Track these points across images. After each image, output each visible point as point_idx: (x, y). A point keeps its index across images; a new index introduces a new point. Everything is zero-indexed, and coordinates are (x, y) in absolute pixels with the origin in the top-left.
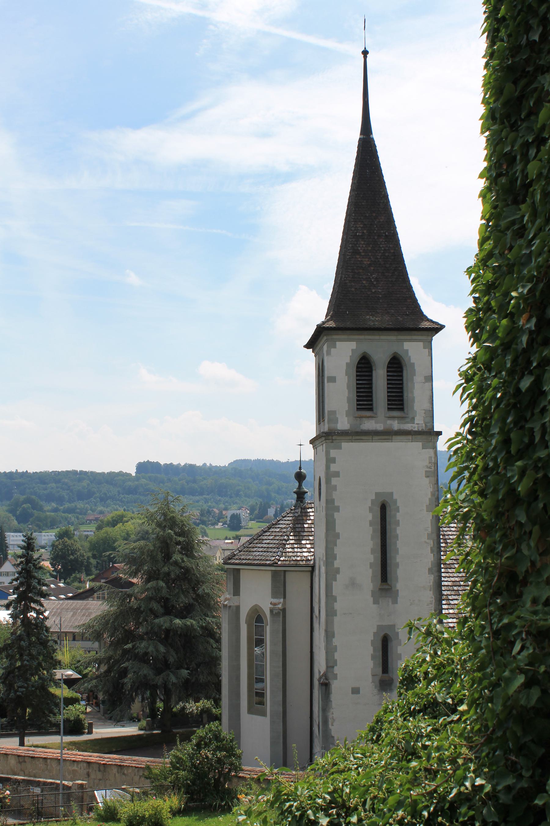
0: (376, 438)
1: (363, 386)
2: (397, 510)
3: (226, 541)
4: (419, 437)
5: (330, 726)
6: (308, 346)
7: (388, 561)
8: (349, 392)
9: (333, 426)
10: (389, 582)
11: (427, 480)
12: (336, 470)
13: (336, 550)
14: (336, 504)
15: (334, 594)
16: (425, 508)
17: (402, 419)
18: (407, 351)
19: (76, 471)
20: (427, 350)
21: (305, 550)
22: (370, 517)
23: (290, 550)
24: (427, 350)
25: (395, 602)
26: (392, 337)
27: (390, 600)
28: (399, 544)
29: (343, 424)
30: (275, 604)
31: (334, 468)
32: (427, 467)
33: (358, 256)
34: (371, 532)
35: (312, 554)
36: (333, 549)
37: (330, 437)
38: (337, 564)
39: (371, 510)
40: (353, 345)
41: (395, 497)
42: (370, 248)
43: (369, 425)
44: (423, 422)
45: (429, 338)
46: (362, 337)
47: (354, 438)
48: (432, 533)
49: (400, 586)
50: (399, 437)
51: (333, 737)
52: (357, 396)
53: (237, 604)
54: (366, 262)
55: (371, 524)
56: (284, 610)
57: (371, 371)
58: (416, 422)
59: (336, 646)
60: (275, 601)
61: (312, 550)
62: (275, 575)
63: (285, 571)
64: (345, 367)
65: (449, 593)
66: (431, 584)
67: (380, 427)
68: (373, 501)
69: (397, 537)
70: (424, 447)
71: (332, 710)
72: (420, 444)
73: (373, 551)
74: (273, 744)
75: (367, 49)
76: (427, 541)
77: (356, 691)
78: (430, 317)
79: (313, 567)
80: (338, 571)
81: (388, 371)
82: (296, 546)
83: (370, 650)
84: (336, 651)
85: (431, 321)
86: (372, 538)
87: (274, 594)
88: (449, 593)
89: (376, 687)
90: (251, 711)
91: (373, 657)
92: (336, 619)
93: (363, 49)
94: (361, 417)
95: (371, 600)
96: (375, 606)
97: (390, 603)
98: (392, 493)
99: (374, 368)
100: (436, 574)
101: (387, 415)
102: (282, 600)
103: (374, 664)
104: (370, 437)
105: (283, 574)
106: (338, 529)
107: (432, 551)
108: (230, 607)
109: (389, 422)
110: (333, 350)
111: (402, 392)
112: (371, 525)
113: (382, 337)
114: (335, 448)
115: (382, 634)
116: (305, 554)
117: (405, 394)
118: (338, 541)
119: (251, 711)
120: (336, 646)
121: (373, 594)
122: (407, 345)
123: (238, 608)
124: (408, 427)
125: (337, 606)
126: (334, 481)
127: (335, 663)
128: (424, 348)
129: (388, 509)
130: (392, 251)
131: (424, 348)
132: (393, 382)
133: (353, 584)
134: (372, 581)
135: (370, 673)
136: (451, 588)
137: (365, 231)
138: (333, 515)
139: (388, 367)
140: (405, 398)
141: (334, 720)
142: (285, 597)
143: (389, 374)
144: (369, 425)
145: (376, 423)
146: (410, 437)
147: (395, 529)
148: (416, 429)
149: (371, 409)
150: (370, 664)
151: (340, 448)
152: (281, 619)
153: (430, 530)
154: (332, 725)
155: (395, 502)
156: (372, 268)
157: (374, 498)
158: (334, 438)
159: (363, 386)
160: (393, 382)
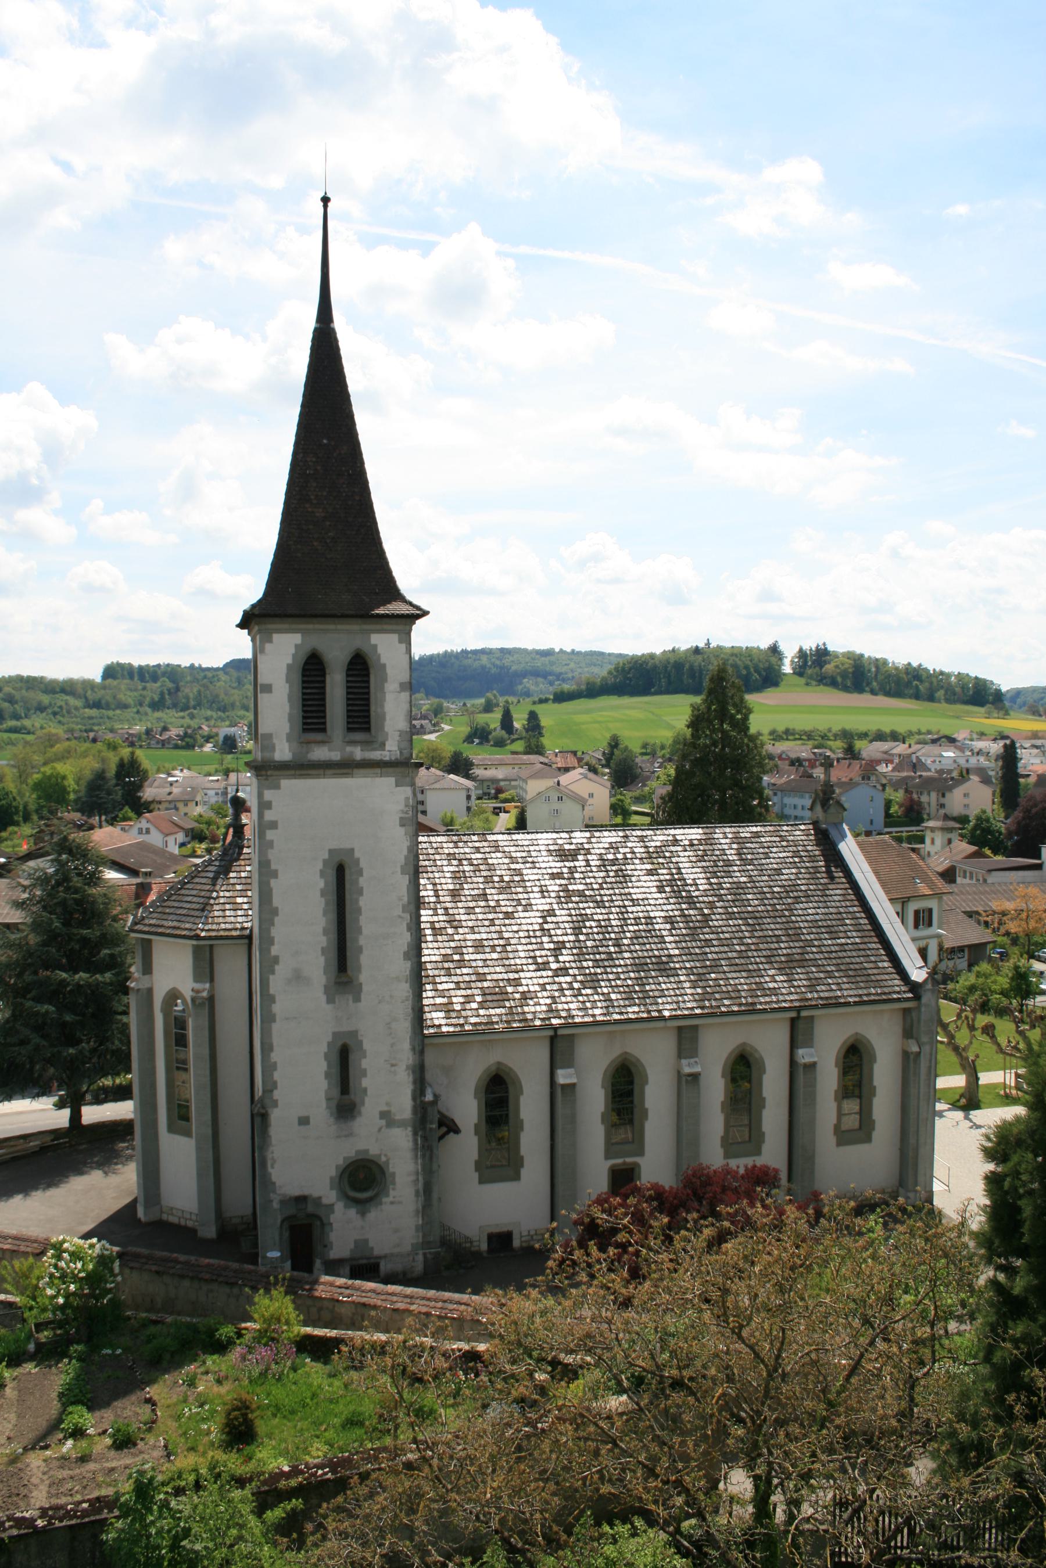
0: (329, 772)
1: (312, 697)
2: (360, 873)
3: (211, 778)
4: (390, 770)
5: (270, 1170)
6: (242, 625)
7: (348, 944)
8: (291, 707)
9: (267, 755)
10: (349, 972)
11: (402, 830)
12: (273, 819)
13: (275, 932)
14: (273, 867)
15: (272, 991)
16: (399, 870)
17: (367, 744)
18: (375, 647)
19: (22, 677)
20: (403, 646)
21: (240, 913)
22: (321, 884)
23: (220, 913)
24: (403, 646)
25: (357, 999)
26: (355, 626)
27: (350, 998)
28: (363, 920)
29: (283, 752)
30: (198, 991)
31: (269, 816)
32: (402, 811)
33: (307, 505)
34: (323, 905)
35: (250, 918)
36: (269, 931)
37: (263, 773)
38: (275, 950)
39: (322, 874)
40: (296, 638)
41: (357, 854)
42: (325, 494)
43: (320, 753)
44: (396, 748)
45: (408, 627)
46: (311, 626)
47: (297, 772)
48: (409, 903)
49: (364, 977)
50: (362, 771)
51: (274, 1183)
52: (304, 711)
53: (147, 986)
54: (319, 513)
55: (323, 893)
56: (211, 999)
57: (324, 675)
58: (387, 748)
59: (275, 1063)
60: (198, 986)
61: (250, 912)
62: (197, 951)
63: (211, 946)
64: (284, 670)
65: (436, 972)
66: (408, 973)
67: (336, 756)
68: (325, 862)
69: (359, 911)
70: (398, 784)
71: (271, 1149)
72: (392, 780)
73: (325, 932)
74: (200, 1175)
75: (329, 195)
76: (403, 915)
77: (304, 1121)
78: (409, 598)
79: (250, 937)
80: (276, 960)
81: (348, 675)
82: (228, 906)
83: (323, 1066)
84: (275, 1069)
85: (411, 604)
86: (325, 913)
87: (198, 977)
88: (436, 972)
89: (332, 1114)
90: (171, 1129)
91: (327, 1075)
92: (276, 1027)
93: (323, 194)
94: (309, 742)
95: (324, 998)
96: (330, 1006)
97: (351, 1002)
98: (352, 850)
99: (327, 671)
100: (415, 960)
101: (347, 739)
102: (207, 986)
103: (329, 1084)
104: (321, 772)
105: (208, 949)
106: (276, 902)
107: (409, 929)
108: (138, 990)
109: (349, 749)
110: (268, 646)
111: (368, 705)
112: (322, 895)
113: (339, 627)
114: (269, 788)
115: (339, 1044)
116: (240, 919)
117: (373, 708)
118: (276, 919)
119: (171, 1129)
120: (275, 1063)
121: (327, 990)
122: (376, 639)
123: (150, 991)
124: (376, 755)
125: (276, 1008)
126: (270, 835)
127: (275, 1085)
128: (400, 642)
129: (347, 872)
130: (357, 498)
131: (400, 642)
132: (356, 690)
133: (298, 977)
134: (325, 973)
135: (323, 1096)
136: (440, 965)
137: (319, 468)
138: (268, 883)
139: (348, 670)
140: (372, 714)
141: (274, 1161)
142: (212, 980)
143: (350, 679)
144: (320, 753)
145: (330, 750)
146: (378, 771)
147: (357, 901)
148: (387, 758)
149: (324, 730)
150: (323, 1084)
151: (277, 787)
152: (207, 1011)
153: (406, 899)
154: (273, 1167)
155: (358, 861)
156: (328, 523)
157: (326, 856)
158: (269, 773)
159: (312, 697)
160: (356, 690)
